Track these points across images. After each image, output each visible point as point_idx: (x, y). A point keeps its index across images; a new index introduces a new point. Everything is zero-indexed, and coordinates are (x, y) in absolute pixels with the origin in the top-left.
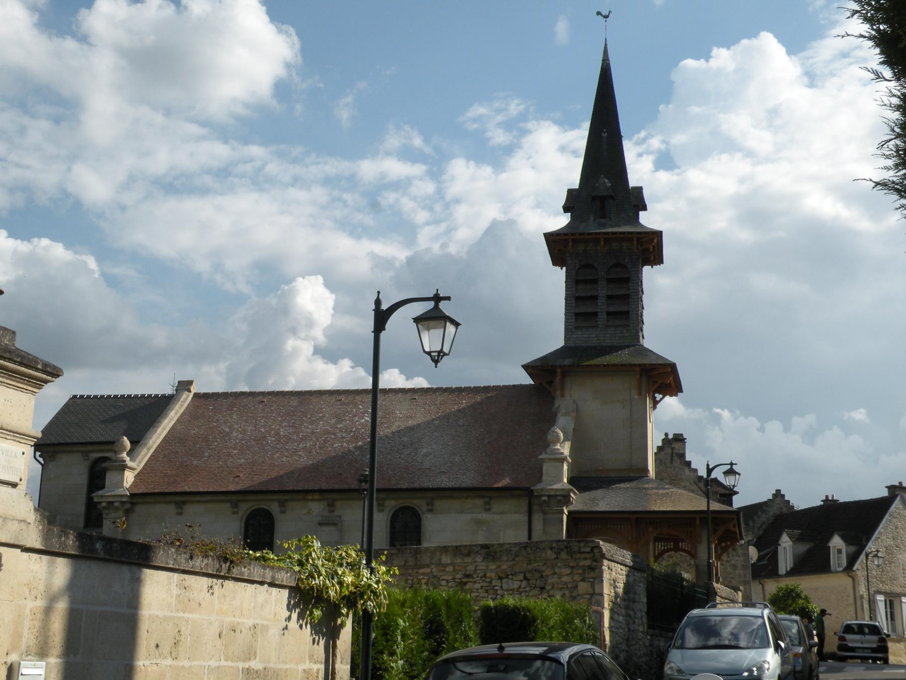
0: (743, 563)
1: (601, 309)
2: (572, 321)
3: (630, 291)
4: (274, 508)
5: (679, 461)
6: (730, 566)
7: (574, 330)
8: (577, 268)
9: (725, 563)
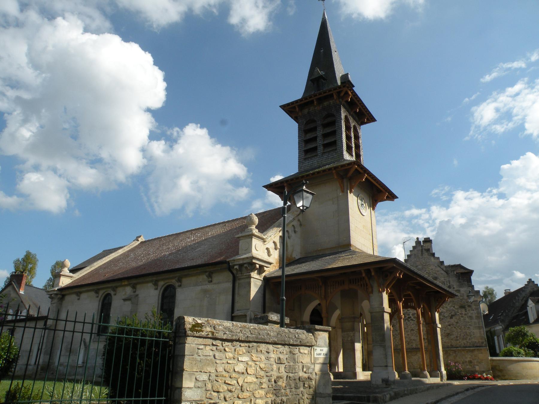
0: (476, 315)
2: (302, 156)
3: (336, 128)
4: (112, 293)
5: (427, 254)
6: (467, 317)
7: (304, 161)
8: (304, 123)
9: (464, 315)
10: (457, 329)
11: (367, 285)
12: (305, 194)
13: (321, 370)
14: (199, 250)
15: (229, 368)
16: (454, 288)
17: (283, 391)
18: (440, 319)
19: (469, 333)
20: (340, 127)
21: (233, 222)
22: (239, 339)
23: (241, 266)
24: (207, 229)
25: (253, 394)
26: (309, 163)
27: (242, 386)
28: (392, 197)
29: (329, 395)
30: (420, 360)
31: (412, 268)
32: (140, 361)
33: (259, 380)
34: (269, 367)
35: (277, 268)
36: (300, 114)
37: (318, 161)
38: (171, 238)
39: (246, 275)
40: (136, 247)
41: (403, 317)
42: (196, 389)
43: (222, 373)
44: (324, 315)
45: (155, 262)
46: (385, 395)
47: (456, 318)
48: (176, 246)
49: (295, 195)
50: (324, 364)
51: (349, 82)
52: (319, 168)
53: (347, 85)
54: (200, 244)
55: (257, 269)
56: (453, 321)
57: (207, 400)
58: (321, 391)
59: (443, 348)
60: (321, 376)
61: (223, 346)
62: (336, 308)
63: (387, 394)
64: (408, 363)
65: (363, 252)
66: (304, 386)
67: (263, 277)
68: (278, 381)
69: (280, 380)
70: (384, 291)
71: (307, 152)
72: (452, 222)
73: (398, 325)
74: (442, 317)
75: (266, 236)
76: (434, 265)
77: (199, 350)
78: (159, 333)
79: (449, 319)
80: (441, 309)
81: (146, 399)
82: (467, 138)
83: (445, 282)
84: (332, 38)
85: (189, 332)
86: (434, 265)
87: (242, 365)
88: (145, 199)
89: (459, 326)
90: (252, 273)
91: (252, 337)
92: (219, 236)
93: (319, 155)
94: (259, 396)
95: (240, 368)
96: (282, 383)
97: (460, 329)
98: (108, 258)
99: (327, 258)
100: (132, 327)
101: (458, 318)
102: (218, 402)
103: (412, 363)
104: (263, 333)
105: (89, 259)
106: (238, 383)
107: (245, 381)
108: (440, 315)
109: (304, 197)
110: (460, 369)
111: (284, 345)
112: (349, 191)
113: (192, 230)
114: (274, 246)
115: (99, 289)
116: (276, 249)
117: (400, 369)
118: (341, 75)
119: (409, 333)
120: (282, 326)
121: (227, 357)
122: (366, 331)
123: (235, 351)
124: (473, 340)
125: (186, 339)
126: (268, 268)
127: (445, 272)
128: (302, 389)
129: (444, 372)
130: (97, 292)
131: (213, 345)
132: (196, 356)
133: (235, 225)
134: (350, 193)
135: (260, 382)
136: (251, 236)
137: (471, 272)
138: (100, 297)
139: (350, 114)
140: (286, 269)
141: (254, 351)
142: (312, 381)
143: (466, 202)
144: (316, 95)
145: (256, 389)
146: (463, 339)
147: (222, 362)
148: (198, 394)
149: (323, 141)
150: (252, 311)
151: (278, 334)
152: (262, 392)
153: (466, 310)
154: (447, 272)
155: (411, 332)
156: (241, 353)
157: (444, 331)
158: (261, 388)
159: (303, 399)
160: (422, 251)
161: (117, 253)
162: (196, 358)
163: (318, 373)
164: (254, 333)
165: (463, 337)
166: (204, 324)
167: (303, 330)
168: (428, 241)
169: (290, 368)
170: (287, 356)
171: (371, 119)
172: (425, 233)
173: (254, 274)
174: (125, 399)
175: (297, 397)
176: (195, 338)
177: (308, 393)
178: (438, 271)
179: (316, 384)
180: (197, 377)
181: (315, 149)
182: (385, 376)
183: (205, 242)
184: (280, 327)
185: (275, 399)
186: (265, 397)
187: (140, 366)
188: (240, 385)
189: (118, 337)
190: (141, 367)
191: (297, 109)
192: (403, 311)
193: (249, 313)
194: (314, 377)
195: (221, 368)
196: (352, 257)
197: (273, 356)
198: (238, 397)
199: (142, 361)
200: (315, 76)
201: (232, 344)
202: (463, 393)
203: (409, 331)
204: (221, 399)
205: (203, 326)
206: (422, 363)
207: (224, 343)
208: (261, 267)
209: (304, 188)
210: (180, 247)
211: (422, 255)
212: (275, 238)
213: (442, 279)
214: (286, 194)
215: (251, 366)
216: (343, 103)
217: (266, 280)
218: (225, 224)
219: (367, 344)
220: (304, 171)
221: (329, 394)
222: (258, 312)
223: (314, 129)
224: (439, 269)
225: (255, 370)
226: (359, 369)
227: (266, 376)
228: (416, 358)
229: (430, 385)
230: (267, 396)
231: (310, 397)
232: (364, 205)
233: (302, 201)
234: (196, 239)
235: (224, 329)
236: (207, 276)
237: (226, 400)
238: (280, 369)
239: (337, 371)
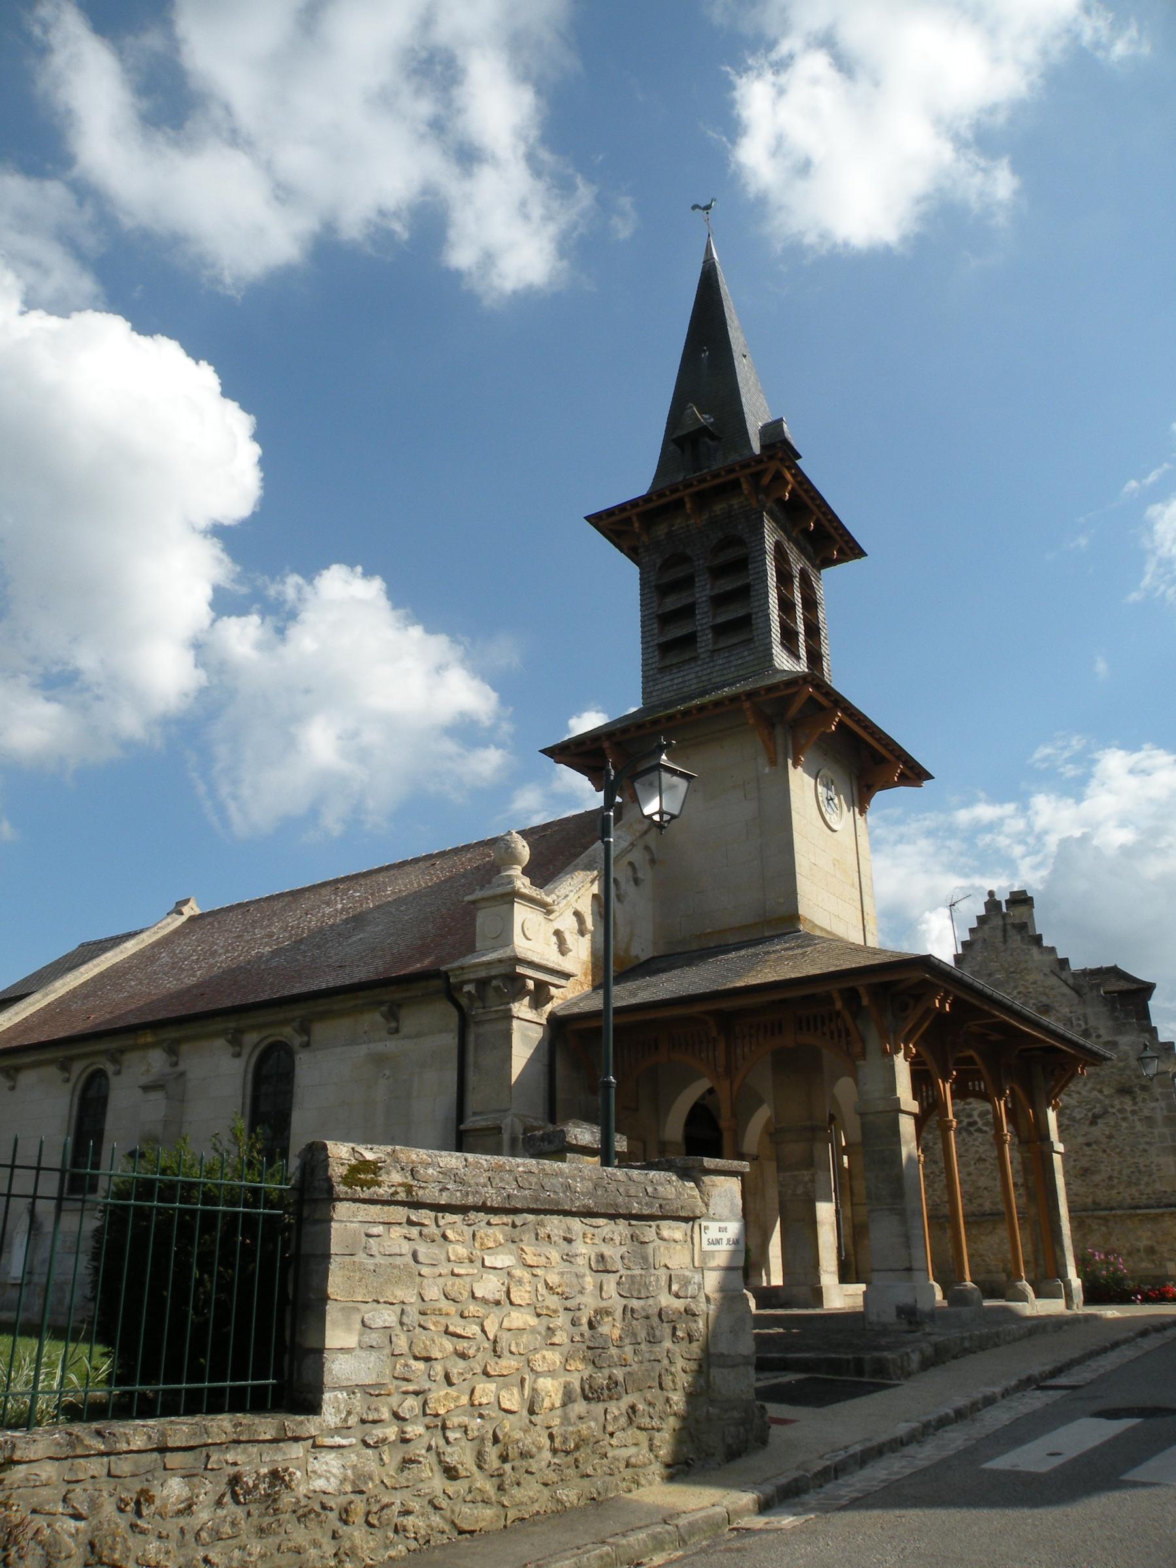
0: (1165, 1113)
1: (701, 625)
4: (110, 1068)
5: (1019, 938)
7: (658, 676)
8: (658, 566)
10: (1109, 1155)
11: (848, 1034)
12: (666, 777)
13: (723, 1288)
14: (361, 939)
15: (457, 1287)
16: (1099, 1036)
17: (614, 1351)
18: (1059, 1126)
19: (1145, 1166)
20: (761, 574)
21: (456, 854)
22: (484, 1203)
23: (482, 983)
24: (380, 878)
25: (529, 1362)
26: (673, 679)
27: (495, 1342)
28: (915, 774)
29: (746, 1361)
30: (1005, 1247)
31: (980, 983)
32: (201, 1274)
33: (545, 1320)
34: (571, 1282)
35: (587, 988)
36: (645, 539)
37: (700, 674)
38: (278, 905)
39: (496, 1011)
40: (176, 932)
41: (954, 1124)
42: (363, 1354)
43: (437, 1303)
44: (724, 1123)
45: (233, 976)
46: (907, 1354)
47: (1107, 1124)
48: (292, 927)
49: (638, 781)
50: (729, 1269)
51: (786, 443)
52: (702, 694)
53: (780, 455)
54: (358, 921)
55: (529, 993)
56: (1097, 1132)
57: (396, 1382)
58: (723, 1347)
59: (1070, 1211)
60: (722, 1305)
61: (438, 1226)
62: (760, 1102)
63: (913, 1351)
64: (970, 1256)
65: (840, 940)
66: (674, 1334)
67: (545, 1016)
68: (599, 1322)
69: (606, 1320)
70: (897, 1052)
71: (665, 648)
72: (1095, 842)
73: (940, 1146)
74: (1066, 1122)
75: (554, 896)
76: (1041, 971)
77: (371, 1240)
78: (255, 1191)
79: (1085, 1128)
80: (1063, 1099)
81: (221, 1384)
82: (1134, 596)
83: (1073, 1019)
84: (734, 317)
85: (341, 1189)
86: (1041, 971)
87: (495, 1279)
88: (201, 789)
89: (1117, 1146)
90: (517, 1004)
91: (521, 1198)
92: (416, 896)
93: (702, 656)
94: (546, 1369)
95: (489, 1287)
96: (611, 1329)
97: (1119, 1154)
98: (95, 966)
99: (730, 956)
100: (176, 1178)
101: (1112, 1123)
102: (426, 1387)
103: (981, 1256)
104: (552, 1184)
105: (39, 971)
106: (483, 1331)
107: (506, 1324)
108: (1059, 1116)
109: (663, 787)
110: (1122, 1270)
111: (613, 1217)
112: (790, 762)
113: (337, 881)
114: (576, 925)
115: (72, 1059)
116: (582, 932)
117: (948, 1276)
118: (760, 424)
119: (972, 1169)
120: (606, 1162)
121: (452, 1258)
122: (846, 1165)
123: (474, 1239)
124: (1158, 1186)
125: (334, 1207)
126: (561, 990)
127: (1072, 988)
128: (667, 1344)
129: (1076, 1282)
130: (65, 1066)
131: (410, 1223)
132: (361, 1257)
133: (462, 864)
134: (795, 768)
135: (549, 1328)
136: (511, 896)
137: (1147, 989)
138: (73, 1080)
139: (790, 539)
140: (615, 990)
141: (528, 1237)
142: (695, 1321)
143: (1133, 782)
144: (691, 485)
145: (538, 1346)
146: (1129, 1184)
147: (437, 1271)
148: (371, 1366)
149: (714, 616)
150: (515, 1115)
151: (596, 1186)
152: (554, 1357)
153: (1134, 1099)
154: (1077, 990)
155: (977, 1166)
156: (491, 1245)
157: (1072, 1163)
158: (551, 1344)
159: (672, 1374)
160: (1005, 931)
161: (122, 952)
162: (361, 1263)
163: (714, 1296)
164: (526, 1185)
165: (1129, 1177)
166: (385, 1162)
167: (667, 1174)
168: (1021, 900)
169: (633, 1283)
170: (624, 1249)
171: (852, 550)
172: (1014, 873)
173: (521, 1008)
174: (161, 1386)
175: (653, 1368)
176: (358, 1205)
177: (685, 1355)
178: (1052, 989)
179: (708, 1327)
180: (366, 1316)
181: (689, 640)
182: (906, 1299)
183: (376, 915)
184: (602, 1165)
185: (591, 1376)
186: (562, 1370)
187: (201, 1290)
188: (491, 1337)
189: (136, 1207)
190: (205, 1293)
191: (636, 525)
192: (953, 1105)
193: (508, 1120)
194: (701, 1307)
195: (436, 1288)
196: (804, 954)
197: (584, 1251)
198: (486, 1373)
199: (206, 1276)
200: (687, 428)
201: (464, 1220)
202: (1133, 1343)
203: (972, 1163)
204: (438, 1379)
205: (380, 1168)
206: (1009, 1256)
207: (443, 1218)
208: (541, 986)
209: (664, 760)
210: (303, 932)
211: (1005, 942)
212: (580, 901)
213: (1065, 1010)
214: (612, 778)
215: (520, 1282)
216: (768, 505)
217: (558, 1026)
218: (432, 862)
219: (852, 1205)
220: (659, 706)
221: (745, 1357)
222: (533, 1118)
223: (686, 583)
224: (1053, 981)
225: (534, 1293)
226: (829, 1277)
227: (566, 1309)
228: (994, 1241)
229: (1035, 1322)
230: (568, 1368)
231: (693, 1366)
232: (836, 801)
233: (658, 798)
234: (351, 908)
235: (441, 1176)
236: (384, 1016)
237: (450, 1383)
238: (605, 1288)
239: (765, 1284)
